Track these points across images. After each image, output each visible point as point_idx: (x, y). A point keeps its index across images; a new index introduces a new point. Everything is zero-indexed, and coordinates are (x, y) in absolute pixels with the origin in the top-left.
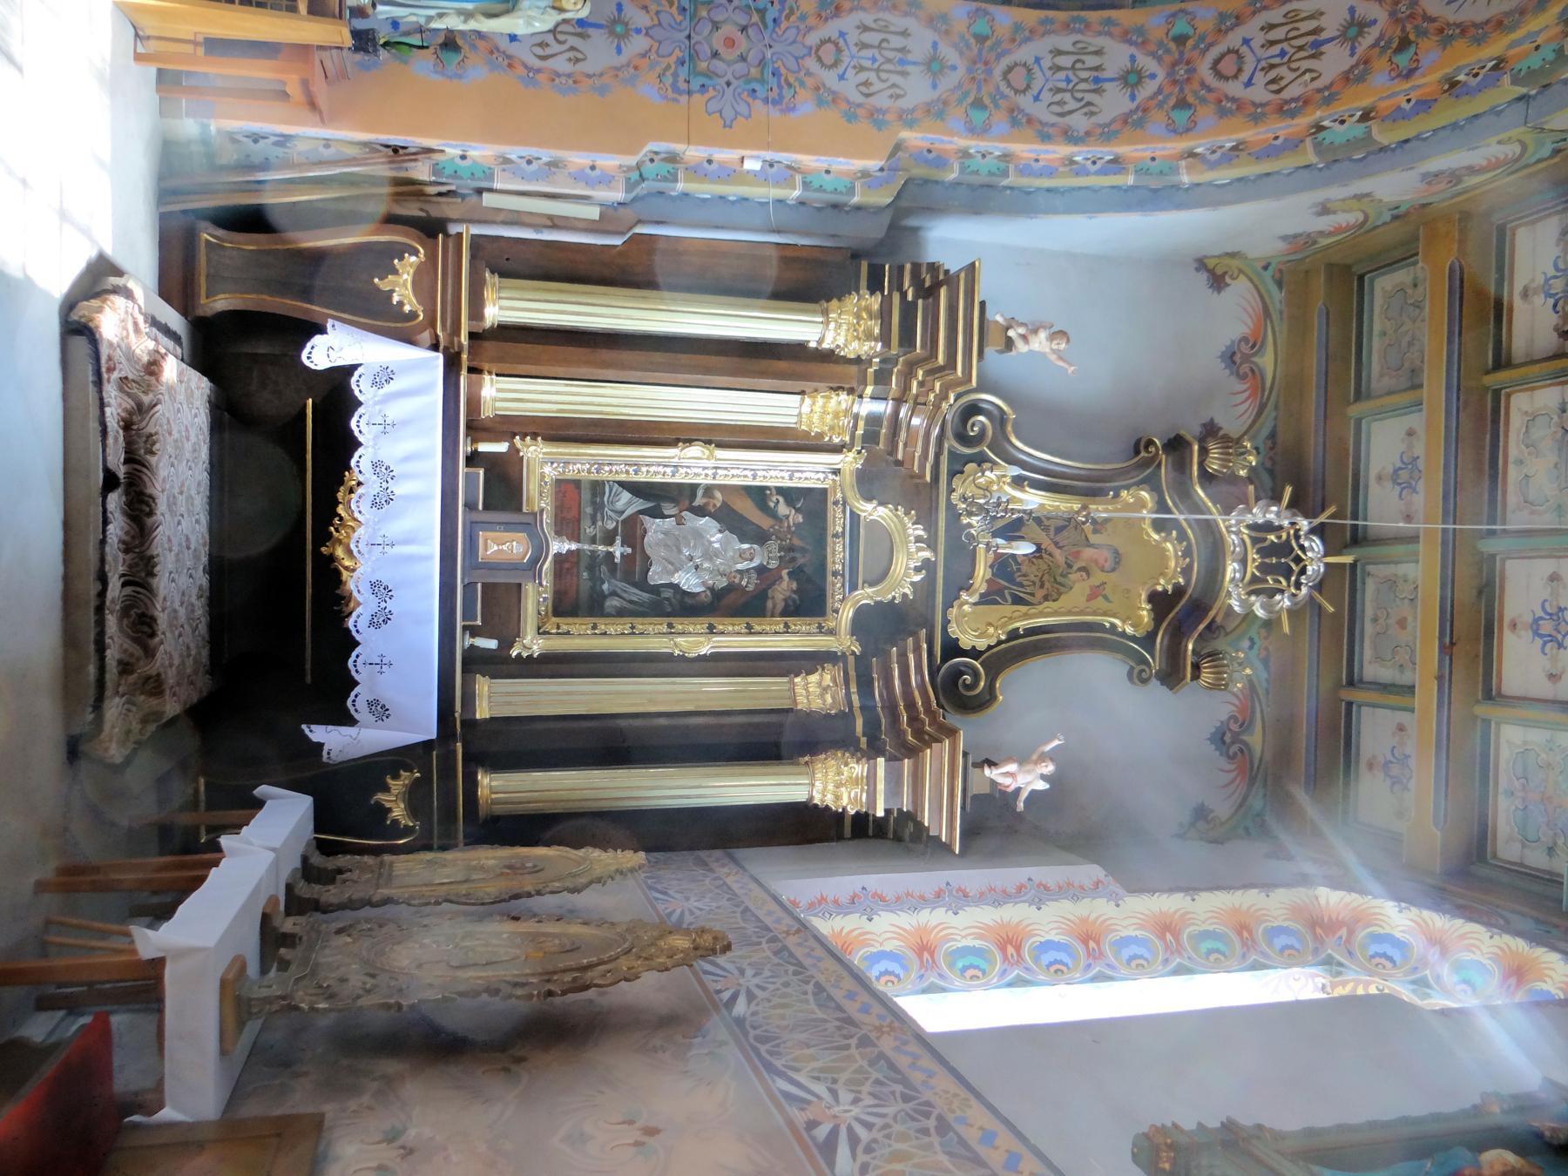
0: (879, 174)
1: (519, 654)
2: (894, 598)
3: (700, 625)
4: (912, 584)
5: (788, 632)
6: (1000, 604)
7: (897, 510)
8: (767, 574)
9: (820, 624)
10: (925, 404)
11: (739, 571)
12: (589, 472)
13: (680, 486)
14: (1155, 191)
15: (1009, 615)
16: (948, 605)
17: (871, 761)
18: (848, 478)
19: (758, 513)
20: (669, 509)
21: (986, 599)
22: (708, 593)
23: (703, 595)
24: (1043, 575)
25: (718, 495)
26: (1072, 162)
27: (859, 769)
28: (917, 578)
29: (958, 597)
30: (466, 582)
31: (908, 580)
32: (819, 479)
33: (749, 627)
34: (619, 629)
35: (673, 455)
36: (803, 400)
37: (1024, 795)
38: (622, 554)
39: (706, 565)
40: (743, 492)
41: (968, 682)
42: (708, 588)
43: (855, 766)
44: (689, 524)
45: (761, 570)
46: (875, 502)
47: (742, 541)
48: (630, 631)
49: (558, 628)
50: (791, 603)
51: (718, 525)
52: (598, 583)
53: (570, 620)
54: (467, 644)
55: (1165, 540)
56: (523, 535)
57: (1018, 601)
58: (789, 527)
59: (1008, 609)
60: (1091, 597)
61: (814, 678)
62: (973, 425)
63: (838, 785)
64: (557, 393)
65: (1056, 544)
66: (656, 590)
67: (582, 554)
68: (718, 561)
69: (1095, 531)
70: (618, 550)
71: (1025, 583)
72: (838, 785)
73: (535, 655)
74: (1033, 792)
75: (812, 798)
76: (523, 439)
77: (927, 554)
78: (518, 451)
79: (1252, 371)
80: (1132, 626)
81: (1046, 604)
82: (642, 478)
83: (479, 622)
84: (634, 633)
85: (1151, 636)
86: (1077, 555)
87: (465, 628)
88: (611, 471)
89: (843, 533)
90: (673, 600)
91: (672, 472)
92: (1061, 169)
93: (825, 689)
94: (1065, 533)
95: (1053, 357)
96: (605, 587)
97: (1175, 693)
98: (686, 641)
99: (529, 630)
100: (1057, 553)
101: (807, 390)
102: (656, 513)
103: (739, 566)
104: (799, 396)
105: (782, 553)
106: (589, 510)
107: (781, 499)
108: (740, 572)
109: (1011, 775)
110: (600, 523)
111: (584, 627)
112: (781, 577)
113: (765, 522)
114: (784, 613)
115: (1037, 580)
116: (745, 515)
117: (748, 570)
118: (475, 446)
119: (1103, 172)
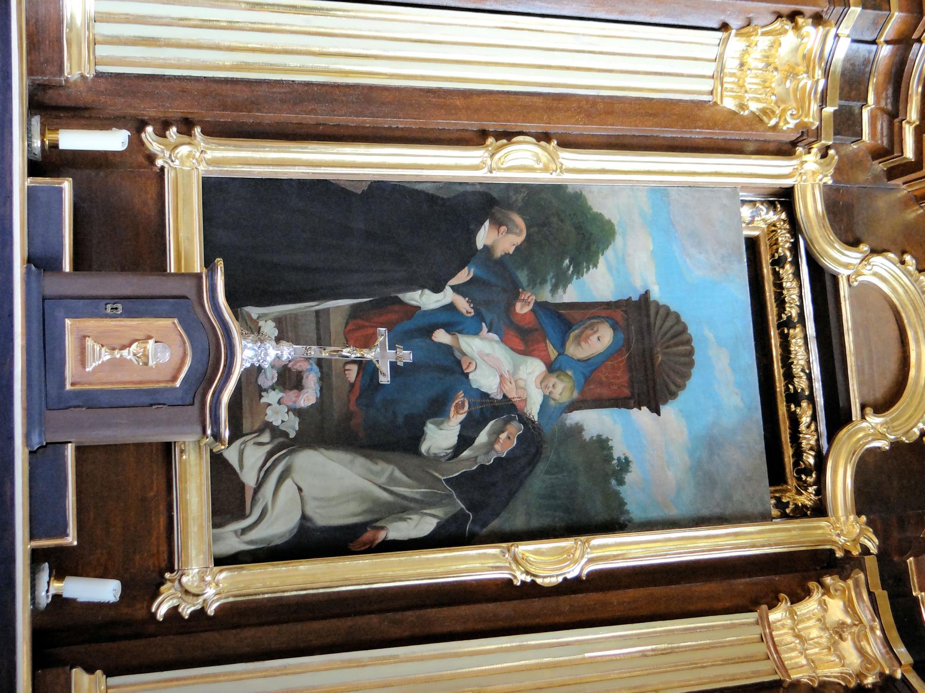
1: (174, 612)
7: (903, 262)
30: (36, 443)
36: (724, 42)
38: (393, 365)
46: (864, 248)
54: (44, 600)
56: (168, 325)
61: (809, 606)
64: (231, 26)
73: (211, 611)
76: (161, 133)
78: (151, 158)
83: (71, 539)
87: (37, 557)
93: (839, 630)
99: (193, 552)
101: (734, 23)
104: (719, 34)
118: (50, 137)
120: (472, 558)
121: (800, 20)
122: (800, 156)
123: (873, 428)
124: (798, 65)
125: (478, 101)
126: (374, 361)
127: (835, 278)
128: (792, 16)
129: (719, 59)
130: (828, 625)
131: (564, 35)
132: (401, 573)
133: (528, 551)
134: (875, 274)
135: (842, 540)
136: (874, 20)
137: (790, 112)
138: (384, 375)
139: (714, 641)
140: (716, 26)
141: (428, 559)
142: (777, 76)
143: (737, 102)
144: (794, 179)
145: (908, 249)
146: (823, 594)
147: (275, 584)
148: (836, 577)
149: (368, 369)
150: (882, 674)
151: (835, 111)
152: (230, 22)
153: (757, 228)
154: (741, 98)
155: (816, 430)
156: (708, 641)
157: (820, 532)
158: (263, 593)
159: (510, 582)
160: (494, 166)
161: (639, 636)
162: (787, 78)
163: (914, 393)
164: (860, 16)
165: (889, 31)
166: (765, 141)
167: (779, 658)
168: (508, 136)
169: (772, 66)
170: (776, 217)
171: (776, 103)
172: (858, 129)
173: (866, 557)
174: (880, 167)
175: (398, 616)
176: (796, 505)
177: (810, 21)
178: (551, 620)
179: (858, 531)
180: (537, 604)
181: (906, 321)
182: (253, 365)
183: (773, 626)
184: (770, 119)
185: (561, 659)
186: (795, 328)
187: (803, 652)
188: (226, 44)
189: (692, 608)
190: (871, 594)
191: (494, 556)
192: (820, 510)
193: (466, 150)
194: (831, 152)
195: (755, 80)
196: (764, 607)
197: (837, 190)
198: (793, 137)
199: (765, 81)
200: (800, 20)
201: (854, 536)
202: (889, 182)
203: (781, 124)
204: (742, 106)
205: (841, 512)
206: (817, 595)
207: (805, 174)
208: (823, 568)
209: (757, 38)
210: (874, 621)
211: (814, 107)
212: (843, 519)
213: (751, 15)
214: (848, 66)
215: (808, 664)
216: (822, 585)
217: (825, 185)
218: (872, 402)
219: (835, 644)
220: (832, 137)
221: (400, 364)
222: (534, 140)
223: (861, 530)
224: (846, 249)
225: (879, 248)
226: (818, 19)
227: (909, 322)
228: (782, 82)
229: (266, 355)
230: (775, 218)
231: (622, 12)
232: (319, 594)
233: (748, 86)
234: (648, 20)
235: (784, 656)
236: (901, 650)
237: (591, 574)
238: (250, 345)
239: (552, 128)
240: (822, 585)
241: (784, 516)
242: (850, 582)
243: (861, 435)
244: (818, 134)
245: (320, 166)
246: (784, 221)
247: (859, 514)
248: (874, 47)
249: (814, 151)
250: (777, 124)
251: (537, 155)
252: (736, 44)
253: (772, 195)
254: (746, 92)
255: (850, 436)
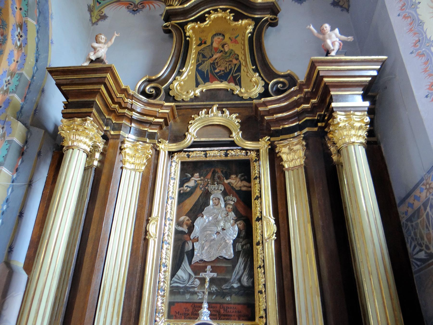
0: (4, 129)
2: (238, 122)
3: (257, 225)
4: (230, 114)
5: (259, 177)
6: (240, 77)
7: (191, 124)
8: (227, 191)
9: (254, 161)
10: (132, 105)
11: (225, 206)
12: (163, 296)
13: (176, 240)
14: (40, 12)
15: (246, 73)
16: (242, 99)
17: (334, 110)
18: (174, 147)
19: (193, 196)
20: (189, 247)
21: (238, 83)
22: (238, 223)
23: (239, 225)
24: (226, 61)
25: (182, 218)
26: (20, 46)
27: (340, 117)
28: (227, 113)
29: (237, 95)
31: (228, 116)
32: (176, 166)
33: (257, 198)
34: (261, 275)
35: (153, 241)
36: (126, 168)
37: (344, 38)
38: (211, 272)
39: (222, 224)
40: (181, 205)
41: (282, 86)
42: (235, 223)
43: (338, 119)
44: (198, 235)
45: (225, 194)
46: (186, 133)
47: (208, 205)
48: (262, 269)
49: (262, 317)
50: (243, 178)
51: (199, 218)
52: (233, 290)
53: (257, 309)
55: (210, 18)
57: (239, 70)
58: (201, 180)
59: (243, 74)
60: (236, 42)
61: (284, 157)
62: (151, 92)
63: (353, 127)
64: (105, 317)
65: (210, 57)
66: (237, 254)
67: (209, 301)
68: (220, 217)
69: (205, 43)
70: (208, 275)
71: (230, 68)
72: (353, 127)
74: (341, 33)
75: (361, 143)
77: (215, 108)
79: (141, 4)
80: (249, 26)
81: (240, 59)
82: (169, 263)
84: (264, 266)
85: (253, 19)
86: (216, 49)
88: (164, 282)
89: (204, 151)
90: (243, 243)
91: (166, 244)
92: (23, 51)
93: (290, 149)
94: (206, 54)
95: (110, 44)
96: (235, 285)
97: (281, 10)
98: (267, 232)
100: (215, 57)
101: (121, 165)
102: (191, 254)
103: (223, 206)
104: (124, 170)
105: (216, 183)
106: (188, 297)
107: (186, 185)
108: (226, 205)
109: (333, 43)
110: (196, 289)
111: (261, 300)
112: (229, 183)
113: (198, 193)
114: (249, 181)
115: (228, 64)
116: (194, 203)
117: (225, 201)
119: (26, 32)
120: (268, 251)
121: (122, 147)
122: (160, 149)
123: (236, 135)
124: (135, 148)
125: (135, 241)
126: (210, 278)
127: (194, 142)
128: (121, 149)
129: (131, 170)
130: (289, 152)
131: (122, 224)
132: (272, 273)
133: (267, 234)
134: (194, 131)
135: (266, 146)
136: (124, 127)
137: (148, 151)
138: (214, 275)
139: (293, 183)
140: (121, 170)
141: (268, 265)
142: (137, 154)
143: (143, 166)
144: (166, 151)
145: (188, 122)
146: (281, 153)
147: (274, 313)
148: (276, 149)
149: (212, 281)
150: (303, 140)
151: (148, 139)
152: (104, 317)
153: (178, 161)
154: (142, 164)
155: (236, 150)
156: (293, 185)
157: (263, 152)
158: (277, 317)
159: (275, 240)
160: (155, 237)
161: (291, 204)
162: (138, 152)
163: (227, 124)
164: (123, 131)
165: (128, 123)
166: (155, 158)
167: (298, 166)
168: (146, 232)
169: (134, 155)
170: (176, 156)
171: (145, 155)
172: (154, 133)
173: (271, 140)
174: (164, 128)
175: (284, 275)
176: (256, 157)
177: (123, 145)
178: (287, 234)
179: (264, 142)
180: (282, 233)
181: (207, 124)
182: (209, 317)
183: (289, 167)
184: (149, 157)
185: (297, 227)
186: (207, 153)
187: (296, 160)
188: (111, 319)
189: (284, 189)
190: (281, 140)
191: (268, 244)
192: (258, 151)
193: (149, 245)
194: (159, 140)
195: (138, 161)
196: (284, 169)
197: (170, 139)
198: (154, 150)
199: (138, 158)
200: (122, 147)
201: (265, 143)
202: (169, 125)
203: (150, 154)
204: (145, 164)
205: (258, 146)
206: (281, 154)
207: (165, 148)
208: (273, 152)
209: (126, 159)
210: (288, 140)
211: (147, 145)
212: (260, 145)
213: (119, 160)
214: (136, 135)
215: (300, 159)
216: (278, 153)
217: (168, 143)
218: (229, 135)
219: (294, 151)
220: (155, 140)
221: (211, 270)
222: (148, 224)
223: (263, 141)
224: (187, 138)
225: (187, 129)
226: (123, 142)
227: (208, 123)
228: (139, 153)
229: (206, 312)
230: (176, 156)
231: (114, 197)
232: (277, 299)
233: (139, 162)
234: (117, 189)
235: (297, 165)
236: (296, 134)
237: (274, 216)
238: (203, 317)
239: (145, 218)
240: (278, 153)
241: (259, 160)
242: (277, 145)
243: (238, 139)
244: (154, 144)
245: (150, 291)
246: (177, 154)
247: (259, 141)
248: (132, 127)
249: (158, 145)
250: (150, 155)
251: (153, 224)
252: (127, 165)
253: (170, 156)
254: (141, 163)
255: (238, 141)
